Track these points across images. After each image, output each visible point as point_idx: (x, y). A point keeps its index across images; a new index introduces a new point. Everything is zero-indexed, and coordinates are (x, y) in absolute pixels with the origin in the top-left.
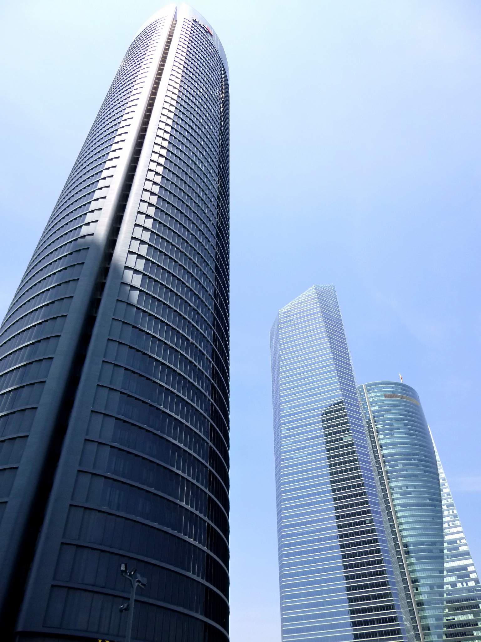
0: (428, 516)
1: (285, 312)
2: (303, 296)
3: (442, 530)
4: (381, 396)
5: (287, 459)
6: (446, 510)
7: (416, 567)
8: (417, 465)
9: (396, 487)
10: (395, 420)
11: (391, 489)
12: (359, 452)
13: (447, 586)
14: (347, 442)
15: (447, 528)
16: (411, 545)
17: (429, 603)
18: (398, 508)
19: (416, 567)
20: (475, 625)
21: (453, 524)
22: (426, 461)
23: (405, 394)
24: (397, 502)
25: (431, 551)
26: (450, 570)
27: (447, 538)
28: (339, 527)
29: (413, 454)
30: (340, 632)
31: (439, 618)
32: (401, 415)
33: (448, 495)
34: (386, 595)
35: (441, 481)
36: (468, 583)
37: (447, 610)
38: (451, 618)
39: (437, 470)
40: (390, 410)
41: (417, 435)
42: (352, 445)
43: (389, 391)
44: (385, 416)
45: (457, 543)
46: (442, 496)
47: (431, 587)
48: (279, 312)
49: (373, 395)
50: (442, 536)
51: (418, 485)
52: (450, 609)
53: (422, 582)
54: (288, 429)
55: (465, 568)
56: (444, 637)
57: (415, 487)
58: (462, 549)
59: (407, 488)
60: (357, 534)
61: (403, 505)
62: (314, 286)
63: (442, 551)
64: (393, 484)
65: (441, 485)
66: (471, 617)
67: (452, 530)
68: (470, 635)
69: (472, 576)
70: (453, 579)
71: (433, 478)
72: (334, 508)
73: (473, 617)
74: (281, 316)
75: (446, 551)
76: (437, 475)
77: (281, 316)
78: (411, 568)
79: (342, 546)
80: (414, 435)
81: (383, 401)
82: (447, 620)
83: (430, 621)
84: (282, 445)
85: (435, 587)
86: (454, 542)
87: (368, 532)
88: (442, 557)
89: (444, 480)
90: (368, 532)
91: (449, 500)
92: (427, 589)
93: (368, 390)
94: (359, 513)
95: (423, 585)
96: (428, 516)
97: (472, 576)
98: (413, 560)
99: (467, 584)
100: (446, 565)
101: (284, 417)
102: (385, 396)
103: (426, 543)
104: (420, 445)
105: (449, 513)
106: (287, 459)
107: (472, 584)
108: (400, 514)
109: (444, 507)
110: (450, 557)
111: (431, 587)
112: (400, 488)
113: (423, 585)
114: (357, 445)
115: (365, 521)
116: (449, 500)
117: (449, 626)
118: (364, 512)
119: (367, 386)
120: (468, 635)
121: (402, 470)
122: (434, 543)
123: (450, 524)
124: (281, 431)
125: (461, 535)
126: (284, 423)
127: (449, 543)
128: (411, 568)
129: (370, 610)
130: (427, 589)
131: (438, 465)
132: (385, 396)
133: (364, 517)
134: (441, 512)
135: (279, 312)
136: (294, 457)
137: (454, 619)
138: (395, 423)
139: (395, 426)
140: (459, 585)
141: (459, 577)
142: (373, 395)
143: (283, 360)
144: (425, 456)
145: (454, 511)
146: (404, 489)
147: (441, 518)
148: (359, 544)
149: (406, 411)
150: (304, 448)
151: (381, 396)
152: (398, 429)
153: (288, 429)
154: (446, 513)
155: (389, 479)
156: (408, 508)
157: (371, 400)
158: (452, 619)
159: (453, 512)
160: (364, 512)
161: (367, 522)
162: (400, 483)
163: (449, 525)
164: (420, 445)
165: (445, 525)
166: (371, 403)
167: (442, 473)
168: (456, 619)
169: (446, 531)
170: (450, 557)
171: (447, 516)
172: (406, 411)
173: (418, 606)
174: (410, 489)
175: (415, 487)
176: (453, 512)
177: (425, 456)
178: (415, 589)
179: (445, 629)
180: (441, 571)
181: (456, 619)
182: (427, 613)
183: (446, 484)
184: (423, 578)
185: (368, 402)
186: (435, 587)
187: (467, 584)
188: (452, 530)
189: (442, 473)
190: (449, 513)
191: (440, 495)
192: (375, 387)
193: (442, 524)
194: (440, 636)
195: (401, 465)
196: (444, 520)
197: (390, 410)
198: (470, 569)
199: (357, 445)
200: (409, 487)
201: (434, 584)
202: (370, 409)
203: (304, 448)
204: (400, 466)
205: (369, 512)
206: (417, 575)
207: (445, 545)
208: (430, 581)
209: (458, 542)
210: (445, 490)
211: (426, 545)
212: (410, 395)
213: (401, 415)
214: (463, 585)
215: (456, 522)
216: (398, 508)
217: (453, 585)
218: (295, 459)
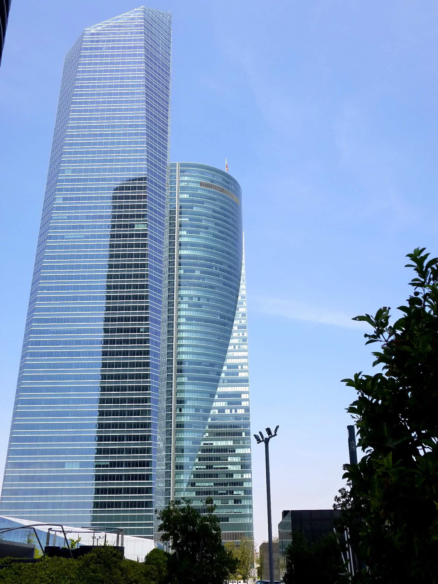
0: (214, 334)
1: (93, 34)
2: (122, 18)
3: (226, 352)
4: (197, 182)
5: (56, 237)
6: (236, 332)
7: (186, 388)
8: (218, 275)
9: (186, 296)
10: (205, 216)
11: (180, 298)
12: (151, 247)
13: (214, 410)
14: (139, 230)
15: (231, 351)
16: (187, 363)
17: (190, 425)
18: (183, 320)
19: (186, 388)
20: (232, 451)
21: (239, 347)
22: (228, 272)
23: (226, 187)
24: (183, 313)
25: (207, 372)
26: (223, 396)
27: (228, 361)
28: (99, 451)
29: (216, 262)
30: (81, 445)
31: (196, 441)
32: (214, 211)
33: (244, 315)
34: (144, 413)
35: (239, 298)
36: (238, 410)
37: (207, 434)
38: (210, 442)
39: (239, 285)
40: (203, 203)
41: (226, 240)
42: (145, 235)
43: (207, 179)
44: (195, 209)
45: (238, 368)
46: (236, 315)
47: (197, 409)
48: (85, 31)
49: (186, 178)
50: (224, 359)
51: (212, 299)
52: (211, 434)
53: (188, 403)
54: (65, 199)
55: (238, 395)
56: (197, 460)
57: (208, 299)
58: (242, 375)
59: (199, 300)
60: (122, 298)
61: (188, 318)
62: (143, 7)
63: (219, 374)
64: (183, 292)
65: (238, 303)
66: (230, 443)
67: (236, 354)
68: (224, 460)
69: (244, 404)
70: (223, 404)
71: (231, 293)
72: (101, 364)
73: (232, 444)
74: (87, 38)
75: (223, 375)
76: (238, 290)
77: (85, 38)
78: (180, 388)
79: (98, 478)
80: (223, 239)
81: (197, 189)
82: (204, 444)
83: (186, 444)
84: (53, 218)
85: (201, 410)
86: (236, 366)
87: (140, 341)
88: (217, 381)
89: (243, 297)
90: (140, 341)
91: (243, 321)
92: (192, 411)
93: (182, 171)
94: (134, 319)
95: (189, 407)
96: (214, 334)
97: (244, 404)
98: (184, 380)
99: (236, 411)
100: (219, 390)
101: (62, 181)
102: (201, 184)
103: (203, 364)
104: (227, 253)
105: (239, 335)
106: (56, 237)
107: (241, 411)
108: (182, 328)
109: (235, 328)
110: (226, 381)
111: (197, 409)
112: (191, 297)
113: (189, 407)
114: (151, 237)
115: (139, 329)
116: (243, 321)
117: (203, 451)
118: (141, 319)
119: (182, 165)
120: (222, 460)
121: (199, 278)
122: (212, 365)
123: (237, 347)
124: (55, 199)
125: (245, 361)
126: (60, 190)
127: (229, 367)
128: (180, 388)
129: (127, 319)
130: (192, 411)
131: (241, 280)
132: (201, 184)
133: (139, 324)
134: (230, 332)
135: (85, 31)
136: (66, 237)
137: (212, 444)
138: (205, 220)
139: (204, 223)
140: (227, 412)
141: (229, 403)
142: (186, 178)
143: (76, 103)
144: (229, 266)
145: (245, 334)
146: (195, 300)
147: (229, 339)
148: (126, 342)
149: (222, 208)
150: (82, 227)
151: (197, 182)
152: (207, 228)
153: (65, 199)
154: (235, 334)
155: (180, 285)
156: (194, 322)
157: (183, 184)
158: (210, 444)
159: (243, 334)
160: (141, 319)
161: (141, 330)
162: (192, 293)
163: (235, 348)
164: (227, 253)
165: (230, 348)
166: (182, 188)
167: (244, 290)
168: (214, 444)
169: (229, 354)
170: (226, 381)
171: (236, 338)
172: (222, 208)
173: (178, 403)
174: (202, 301)
175: (208, 299)
176: (243, 334)
177: (229, 266)
178: (178, 410)
179: (200, 453)
180: (212, 395)
181: (214, 444)
182: (185, 435)
183: (244, 303)
184: (190, 399)
185: (178, 186)
186: (201, 410)
187: (236, 411)
188: (236, 354)
189: (244, 290)
190: (239, 335)
191: (234, 314)
192: (193, 170)
193: (227, 345)
194: (192, 459)
195: (199, 272)
196: (231, 341)
197: (203, 203)
198: (243, 396)
199: (151, 237)
200: (201, 299)
201: (201, 407)
202: (178, 196)
203: (82, 227)
204: (197, 273)
205: (146, 319)
206: (185, 395)
207: (225, 368)
208: (197, 404)
209: (240, 367)
210: (241, 310)
211: (204, 365)
212: (231, 190)
213: (214, 211)
214: (231, 412)
215: (243, 346)
216: (183, 320)
217: (221, 410)
218: (66, 239)
